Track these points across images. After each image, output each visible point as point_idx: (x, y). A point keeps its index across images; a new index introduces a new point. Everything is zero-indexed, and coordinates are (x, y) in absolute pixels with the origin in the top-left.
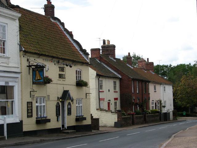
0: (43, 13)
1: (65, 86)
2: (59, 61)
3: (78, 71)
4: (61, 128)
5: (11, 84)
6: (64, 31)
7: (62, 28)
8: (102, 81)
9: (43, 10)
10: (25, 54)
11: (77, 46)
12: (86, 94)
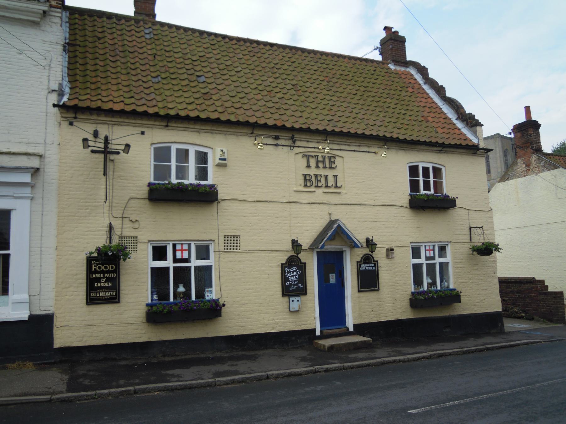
0: (379, 58)
1: (332, 209)
2: (293, 136)
3: (426, 170)
4: (314, 330)
5: (344, 250)
6: (425, 83)
7: (419, 78)
8: (437, 172)
9: (377, 52)
10: (75, 118)
11: (451, 109)
12: (471, 228)
